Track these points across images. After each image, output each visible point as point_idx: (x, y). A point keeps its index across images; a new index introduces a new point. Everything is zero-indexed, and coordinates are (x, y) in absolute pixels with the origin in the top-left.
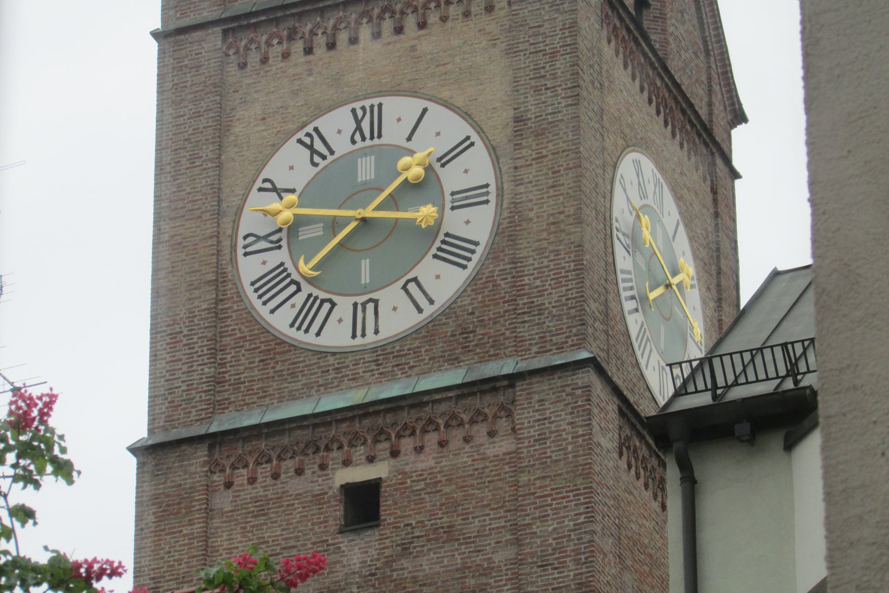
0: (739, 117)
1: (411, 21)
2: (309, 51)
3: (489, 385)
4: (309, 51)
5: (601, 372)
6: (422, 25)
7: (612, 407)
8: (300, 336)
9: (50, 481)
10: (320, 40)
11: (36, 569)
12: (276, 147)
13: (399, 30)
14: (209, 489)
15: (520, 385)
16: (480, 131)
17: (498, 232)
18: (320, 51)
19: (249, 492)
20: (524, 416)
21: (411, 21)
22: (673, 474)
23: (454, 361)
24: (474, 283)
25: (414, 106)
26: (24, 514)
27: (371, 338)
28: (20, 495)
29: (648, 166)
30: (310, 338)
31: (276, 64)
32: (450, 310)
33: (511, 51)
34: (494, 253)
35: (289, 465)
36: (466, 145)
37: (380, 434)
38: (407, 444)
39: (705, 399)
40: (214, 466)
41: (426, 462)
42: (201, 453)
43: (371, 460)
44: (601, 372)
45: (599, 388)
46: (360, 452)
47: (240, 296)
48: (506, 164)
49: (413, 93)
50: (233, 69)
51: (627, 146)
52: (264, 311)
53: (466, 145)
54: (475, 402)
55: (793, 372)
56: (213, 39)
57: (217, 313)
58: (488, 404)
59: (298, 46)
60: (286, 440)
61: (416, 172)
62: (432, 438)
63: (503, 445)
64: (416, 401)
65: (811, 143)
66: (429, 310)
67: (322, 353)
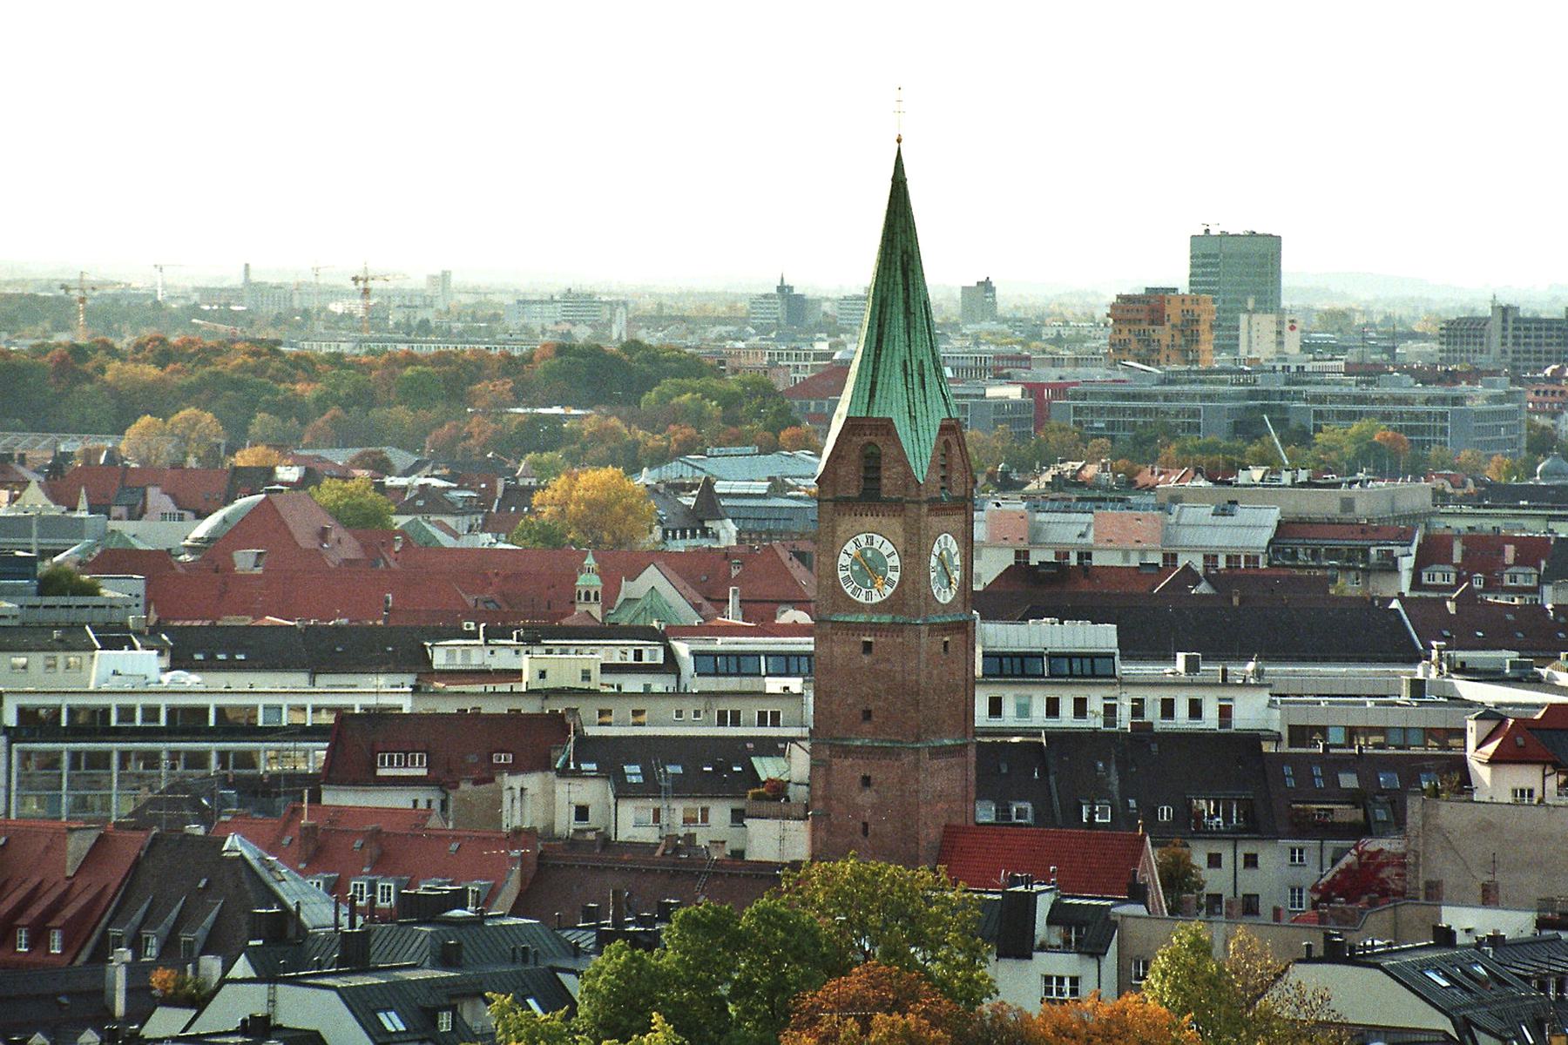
31: (847, 517)
36: (893, 553)
52: (845, 587)
53: (893, 553)
56: (831, 505)
57: (833, 586)
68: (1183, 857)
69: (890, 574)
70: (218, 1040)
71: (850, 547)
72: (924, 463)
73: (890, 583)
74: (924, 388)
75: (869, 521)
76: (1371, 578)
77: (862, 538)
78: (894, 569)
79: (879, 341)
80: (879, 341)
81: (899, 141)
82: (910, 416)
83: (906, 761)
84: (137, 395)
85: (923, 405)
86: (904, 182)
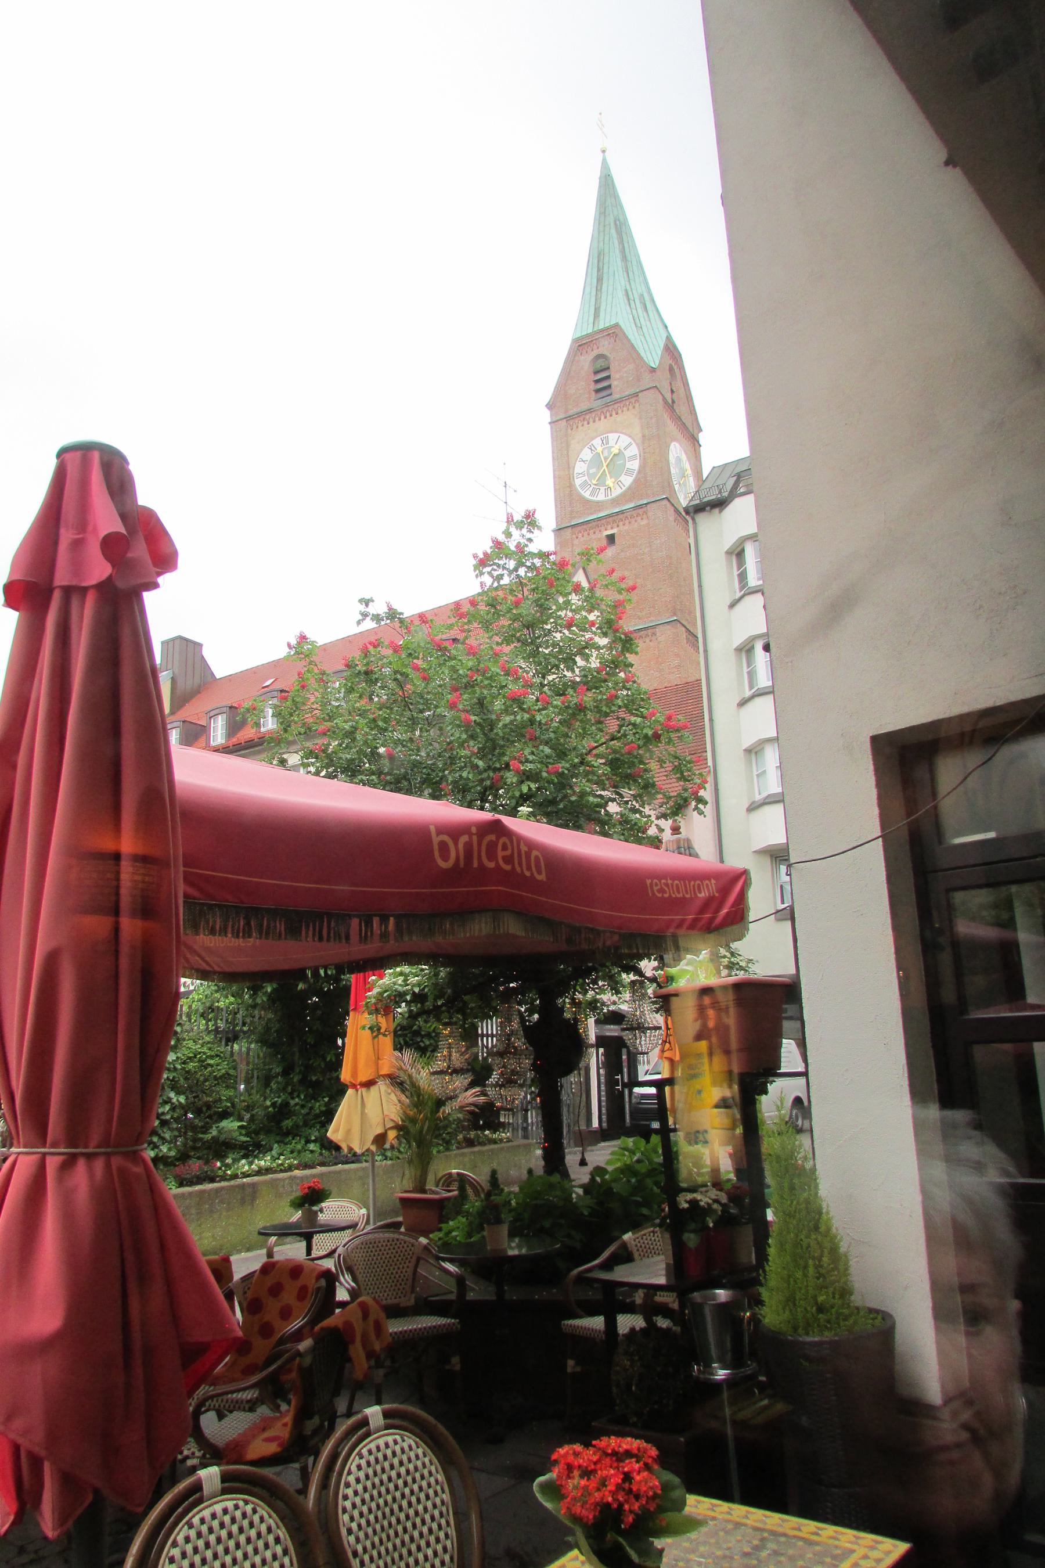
0: (701, 430)
1: (614, 413)
2: (588, 423)
3: (640, 507)
4: (588, 423)
5: (669, 500)
6: (617, 414)
7: (672, 509)
8: (592, 498)
9: (536, 531)
10: (591, 420)
11: (535, 554)
12: (582, 450)
13: (611, 416)
14: (572, 539)
15: (648, 506)
16: (634, 440)
17: (640, 466)
18: (591, 423)
19: (582, 539)
20: (650, 514)
21: (614, 413)
22: (690, 521)
23: (631, 501)
24: (636, 481)
25: (616, 435)
26: (530, 540)
27: (610, 497)
28: (529, 535)
29: (677, 445)
30: (594, 499)
31: (580, 428)
32: (630, 488)
33: (640, 418)
34: (639, 472)
35: (592, 531)
36: (630, 444)
37: (614, 521)
38: (621, 524)
39: (698, 502)
40: (573, 533)
41: (626, 527)
42: (569, 530)
43: (612, 528)
44: (669, 500)
45: (668, 505)
46: (609, 527)
47: (576, 489)
48: (641, 448)
49: (616, 432)
50: (569, 430)
51: (672, 441)
52: (582, 492)
53: (630, 444)
54: (637, 511)
55: (720, 492)
56: (564, 423)
57: (571, 495)
58: (641, 511)
59: (586, 423)
60: (590, 525)
61: (617, 451)
62: (627, 522)
63: (644, 522)
64: (622, 512)
65: (746, 401)
66: (624, 488)
67: (598, 502)
68: (570, 1539)
69: (628, 465)
70: (434, 1298)
71: (586, 454)
72: (655, 356)
73: (629, 472)
74: (647, 312)
75: (602, 424)
76: (723, 1132)
77: (597, 442)
78: (629, 472)
79: (600, 280)
80: (600, 280)
81: (604, 152)
82: (636, 326)
83: (662, 639)
84: (194, 1006)
85: (648, 323)
86: (615, 196)
